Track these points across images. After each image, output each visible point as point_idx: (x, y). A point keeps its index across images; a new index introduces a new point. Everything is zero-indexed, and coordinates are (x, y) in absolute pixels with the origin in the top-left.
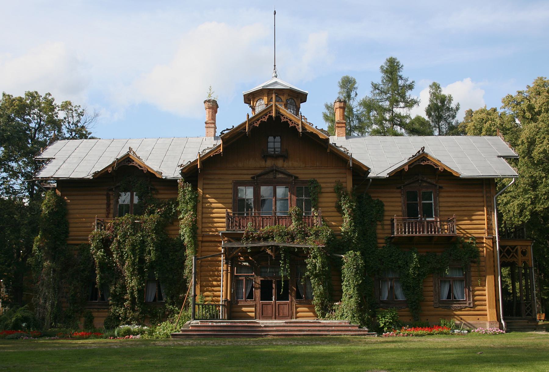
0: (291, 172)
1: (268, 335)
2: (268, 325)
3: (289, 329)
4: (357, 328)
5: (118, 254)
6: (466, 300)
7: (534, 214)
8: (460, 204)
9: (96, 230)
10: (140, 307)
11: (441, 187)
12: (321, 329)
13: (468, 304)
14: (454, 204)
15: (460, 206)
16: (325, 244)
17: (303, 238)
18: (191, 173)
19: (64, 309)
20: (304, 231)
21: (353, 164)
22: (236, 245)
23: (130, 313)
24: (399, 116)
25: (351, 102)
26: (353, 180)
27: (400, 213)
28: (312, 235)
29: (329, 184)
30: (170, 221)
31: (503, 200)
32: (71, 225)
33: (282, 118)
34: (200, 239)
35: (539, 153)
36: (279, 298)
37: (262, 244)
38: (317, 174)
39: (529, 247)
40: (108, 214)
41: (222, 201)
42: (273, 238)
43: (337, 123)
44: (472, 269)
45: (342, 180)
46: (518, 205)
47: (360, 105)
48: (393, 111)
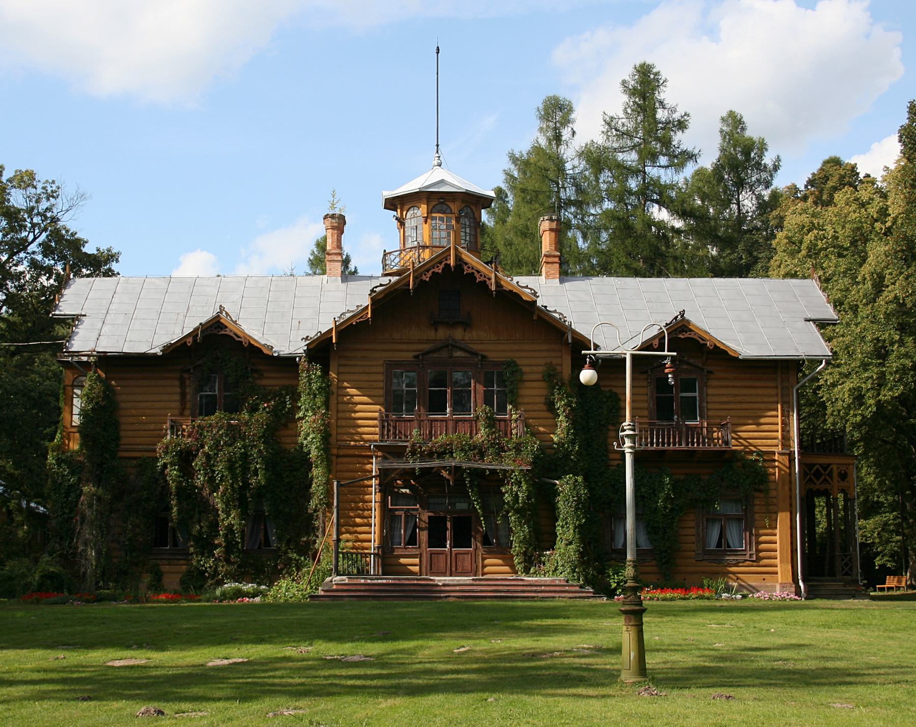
0: (475, 347)
1: (449, 596)
2: (447, 582)
3: (479, 588)
4: (577, 589)
5: (206, 474)
6: (745, 550)
7: (879, 404)
8: (738, 399)
9: (169, 437)
10: (238, 557)
11: (710, 372)
12: (525, 588)
13: (748, 556)
14: (732, 399)
15: (741, 403)
16: (531, 464)
17: (498, 454)
18: (321, 350)
19: (115, 560)
20: (498, 444)
21: (573, 338)
22: (395, 465)
23: (223, 567)
24: (656, 182)
25: (562, 148)
26: (572, 359)
27: (646, 413)
28: (510, 450)
29: (535, 368)
30: (283, 421)
31: (826, 381)
32: (123, 427)
33: (465, 268)
34: (335, 451)
35: (887, 303)
36: (455, 544)
37: (436, 463)
38: (517, 351)
39: (851, 467)
40: (183, 409)
41: (368, 393)
42: (452, 453)
43: (545, 256)
44: (757, 502)
45: (555, 361)
46: (850, 390)
47: (580, 155)
48: (645, 172)
